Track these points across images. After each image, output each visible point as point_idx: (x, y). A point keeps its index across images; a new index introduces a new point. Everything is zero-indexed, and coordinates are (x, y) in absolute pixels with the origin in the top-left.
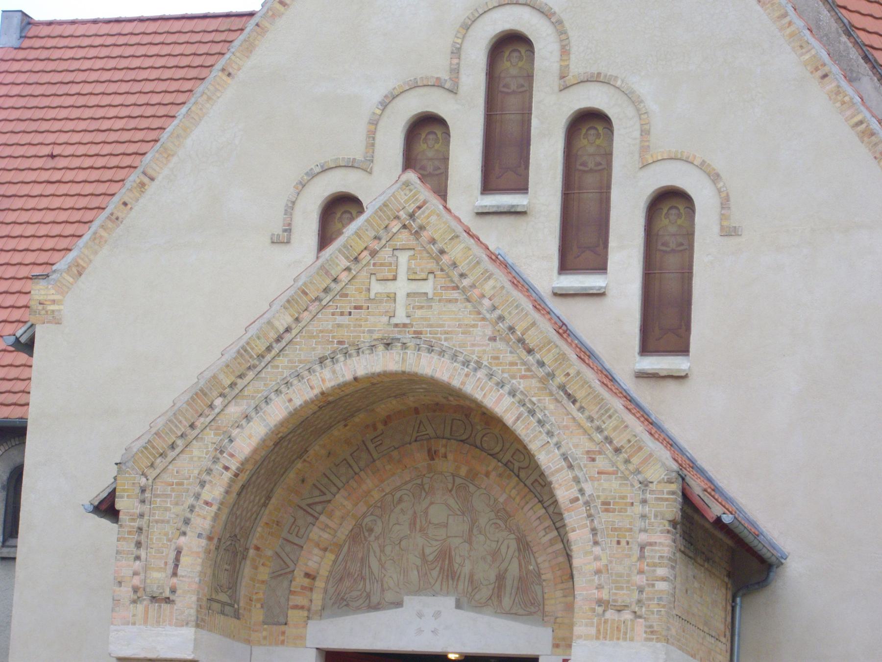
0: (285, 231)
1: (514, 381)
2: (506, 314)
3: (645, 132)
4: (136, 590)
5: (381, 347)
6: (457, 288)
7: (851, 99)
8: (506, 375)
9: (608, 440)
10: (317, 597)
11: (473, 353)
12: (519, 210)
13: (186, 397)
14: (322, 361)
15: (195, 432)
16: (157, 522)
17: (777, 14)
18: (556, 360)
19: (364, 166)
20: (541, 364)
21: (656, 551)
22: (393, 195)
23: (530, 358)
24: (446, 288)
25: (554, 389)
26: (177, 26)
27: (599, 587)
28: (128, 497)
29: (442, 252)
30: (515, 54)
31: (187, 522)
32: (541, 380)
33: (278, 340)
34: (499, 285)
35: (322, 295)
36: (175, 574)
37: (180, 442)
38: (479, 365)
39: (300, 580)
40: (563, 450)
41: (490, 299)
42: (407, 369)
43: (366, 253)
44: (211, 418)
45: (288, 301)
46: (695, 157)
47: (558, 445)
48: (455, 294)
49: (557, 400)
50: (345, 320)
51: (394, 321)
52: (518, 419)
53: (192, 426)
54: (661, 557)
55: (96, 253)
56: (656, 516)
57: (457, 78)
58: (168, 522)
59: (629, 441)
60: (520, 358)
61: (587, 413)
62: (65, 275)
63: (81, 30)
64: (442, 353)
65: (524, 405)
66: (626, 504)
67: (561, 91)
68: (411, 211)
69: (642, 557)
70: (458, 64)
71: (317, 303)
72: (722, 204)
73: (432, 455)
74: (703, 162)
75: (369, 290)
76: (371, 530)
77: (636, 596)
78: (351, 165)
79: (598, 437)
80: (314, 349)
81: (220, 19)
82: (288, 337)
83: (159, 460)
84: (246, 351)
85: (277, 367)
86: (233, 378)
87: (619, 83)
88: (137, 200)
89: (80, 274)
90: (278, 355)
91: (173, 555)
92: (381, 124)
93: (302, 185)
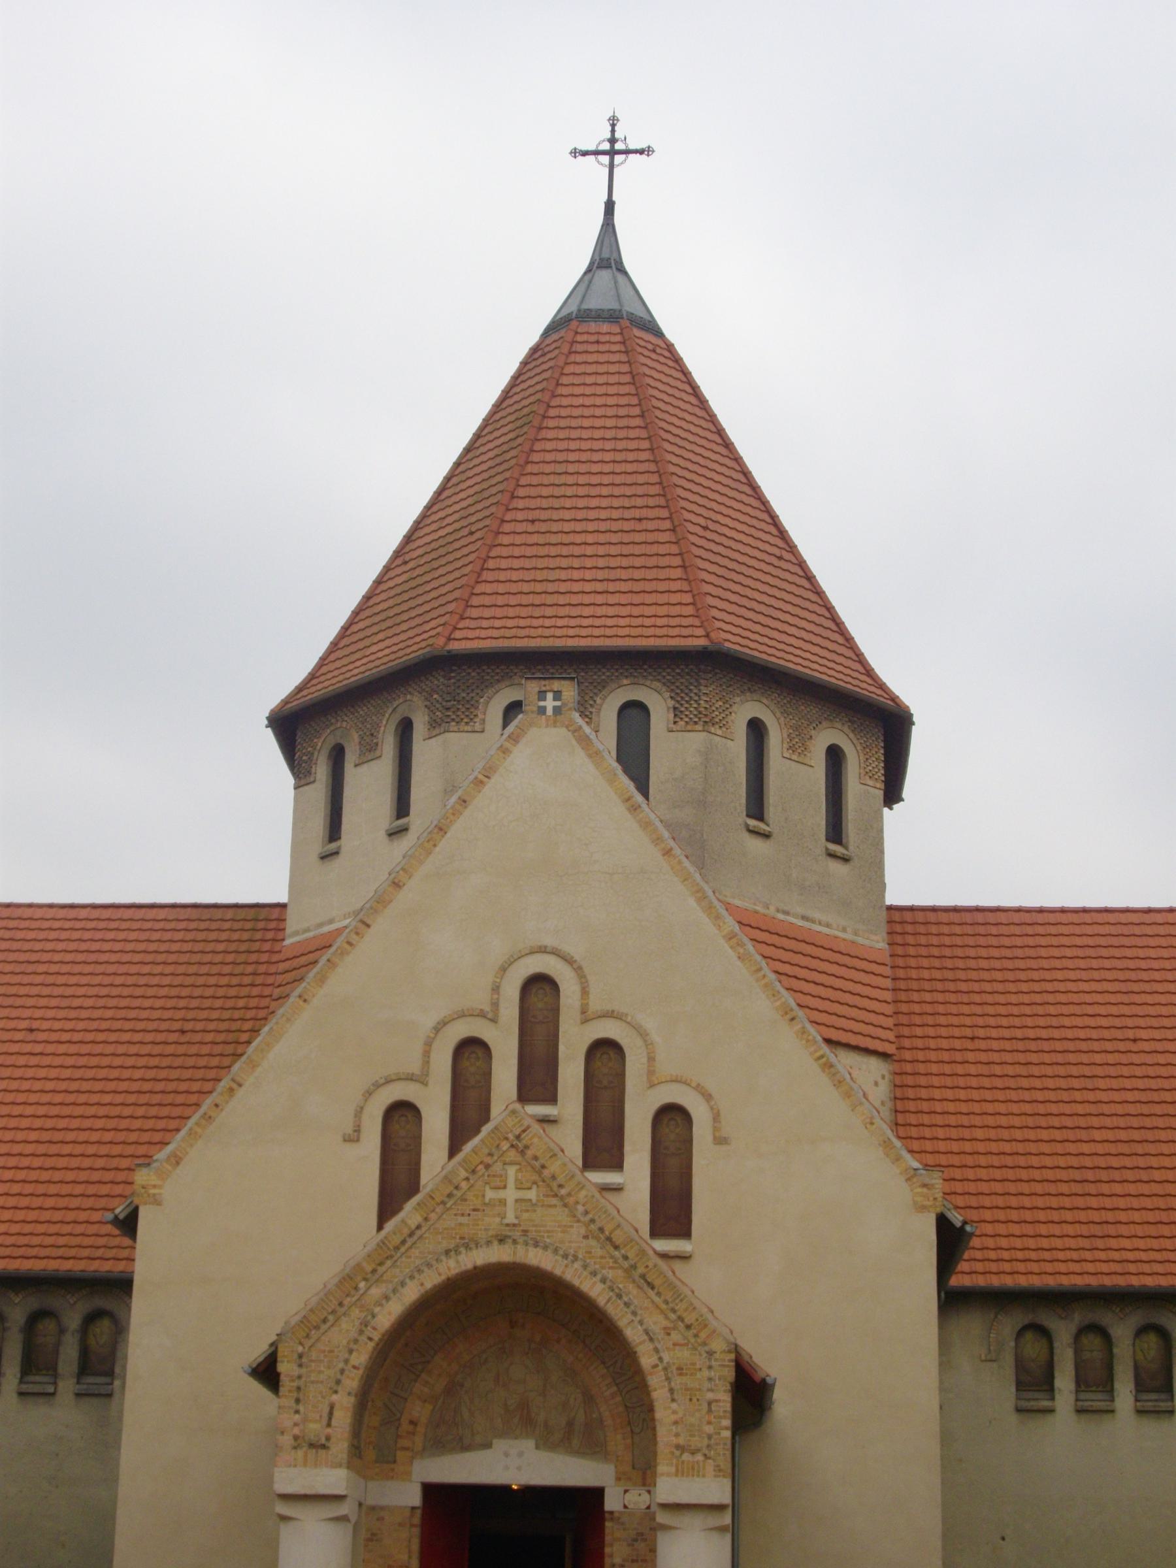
0: (355, 1131)
1: (604, 1271)
2: (596, 1218)
3: (651, 1059)
4: (296, 1438)
5: (496, 1243)
6: (556, 1195)
7: (814, 1037)
8: (597, 1266)
9: (681, 1319)
10: (419, 1440)
11: (571, 1248)
12: (552, 1118)
13: (336, 1280)
14: (447, 1252)
15: (343, 1310)
16: (313, 1382)
17: (754, 968)
18: (637, 1255)
19: (421, 1079)
20: (626, 1258)
21: (720, 1406)
22: (503, 1121)
23: (617, 1253)
24: (547, 1196)
25: (637, 1278)
26: (128, 914)
27: (677, 1435)
28: (288, 1362)
29: (543, 1167)
30: (541, 991)
31: (338, 1382)
32: (626, 1271)
33: (411, 1234)
34: (590, 1194)
35: (446, 1199)
36: (329, 1425)
37: (331, 1318)
38: (576, 1258)
39: (405, 1426)
40: (644, 1327)
41: (584, 1205)
42: (518, 1260)
43: (481, 1167)
44: (354, 1299)
45: (418, 1204)
46: (691, 1080)
47: (641, 1323)
48: (554, 1201)
49: (639, 1287)
50: (464, 1220)
51: (506, 1221)
52: (608, 1301)
53: (341, 1304)
54: (725, 1411)
55: (191, 1146)
56: (720, 1379)
57: (497, 1010)
58: (322, 1382)
59: (697, 1320)
60: (608, 1252)
61: (663, 1297)
62: (165, 1164)
63: (39, 913)
64: (545, 1248)
65: (613, 1290)
66: (695, 1369)
67: (582, 1023)
68: (517, 1133)
69: (710, 1411)
70: (498, 999)
71: (441, 1206)
72: (714, 1119)
73: (513, 1324)
74: (699, 1085)
75: (484, 1196)
76: (462, 1385)
77: (706, 1441)
78: (410, 1078)
79: (673, 1316)
80: (439, 1243)
81: (167, 909)
82: (419, 1233)
83: (313, 1332)
84: (384, 1243)
85: (410, 1257)
86: (374, 1266)
87: (629, 1019)
88: (227, 1102)
89: (178, 1163)
90: (410, 1248)
91: (326, 1410)
92: (435, 1045)
93: (368, 1094)
